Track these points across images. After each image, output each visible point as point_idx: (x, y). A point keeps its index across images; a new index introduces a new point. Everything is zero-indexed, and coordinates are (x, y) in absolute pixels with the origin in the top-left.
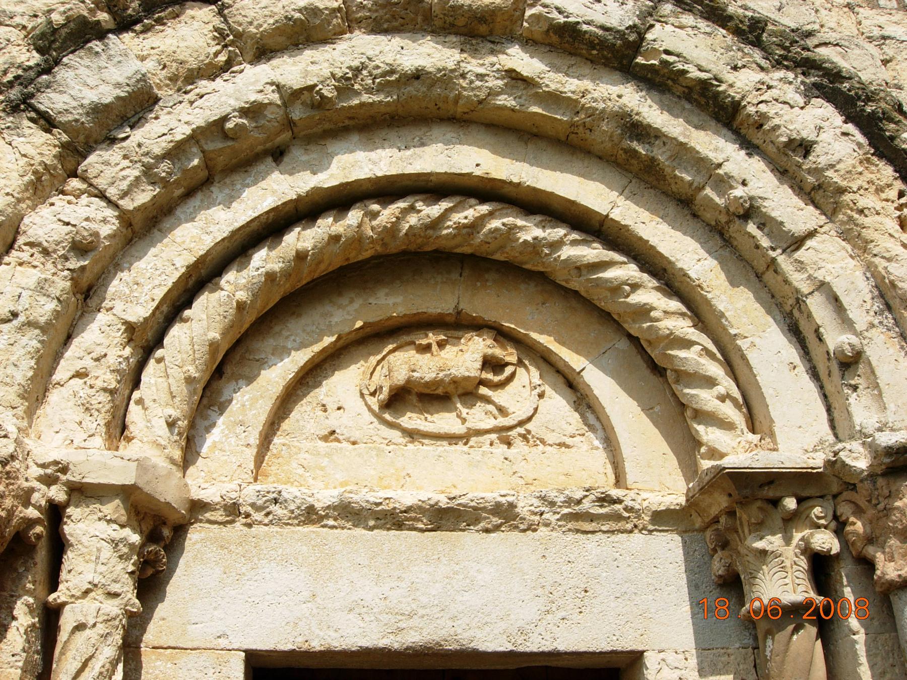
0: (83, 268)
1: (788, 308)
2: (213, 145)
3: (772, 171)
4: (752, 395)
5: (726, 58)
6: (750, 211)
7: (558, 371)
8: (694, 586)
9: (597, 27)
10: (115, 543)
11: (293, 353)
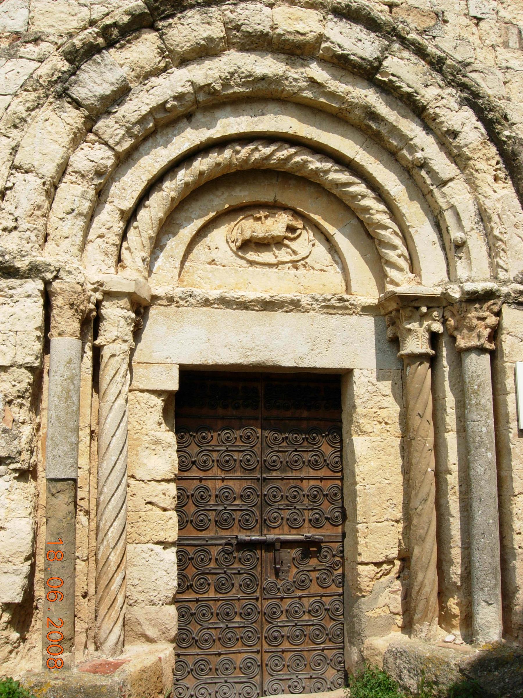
0: (100, 183)
1: (436, 214)
2: (160, 116)
3: (437, 143)
4: (414, 259)
5: (422, 80)
6: (424, 165)
7: (322, 233)
8: (378, 341)
9: (358, 57)
10: (125, 318)
11: (195, 221)
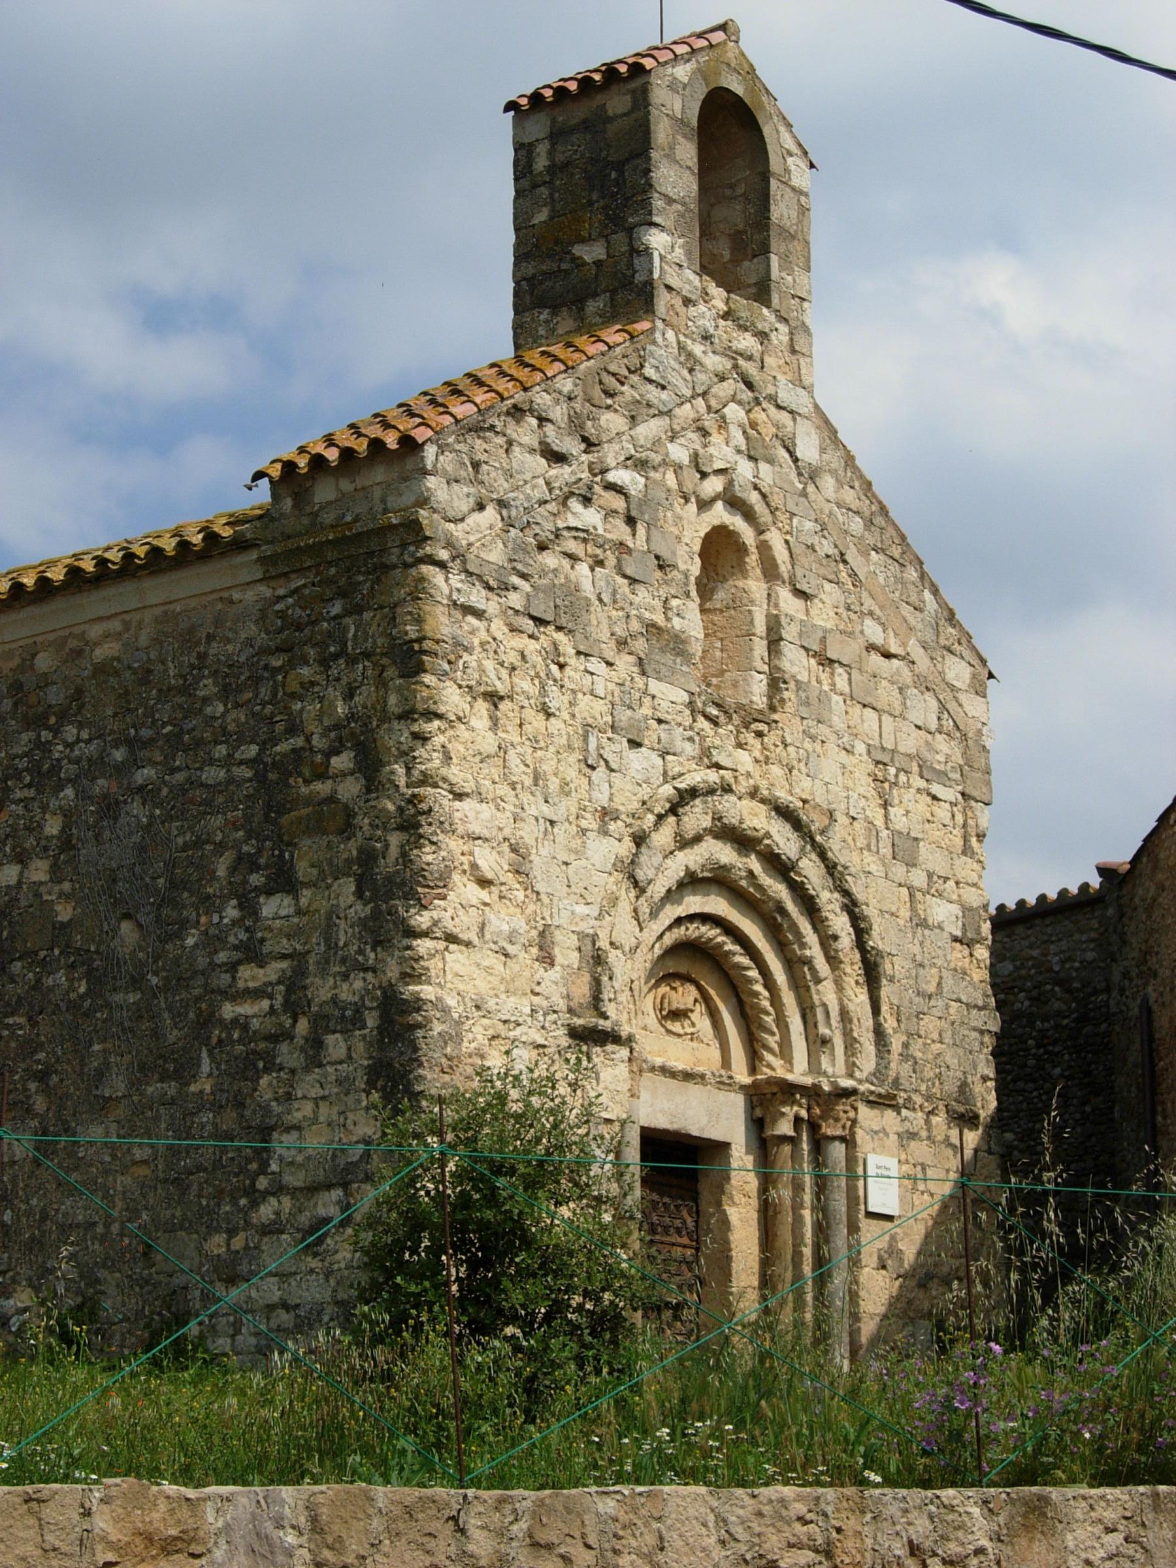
6: (808, 962)
